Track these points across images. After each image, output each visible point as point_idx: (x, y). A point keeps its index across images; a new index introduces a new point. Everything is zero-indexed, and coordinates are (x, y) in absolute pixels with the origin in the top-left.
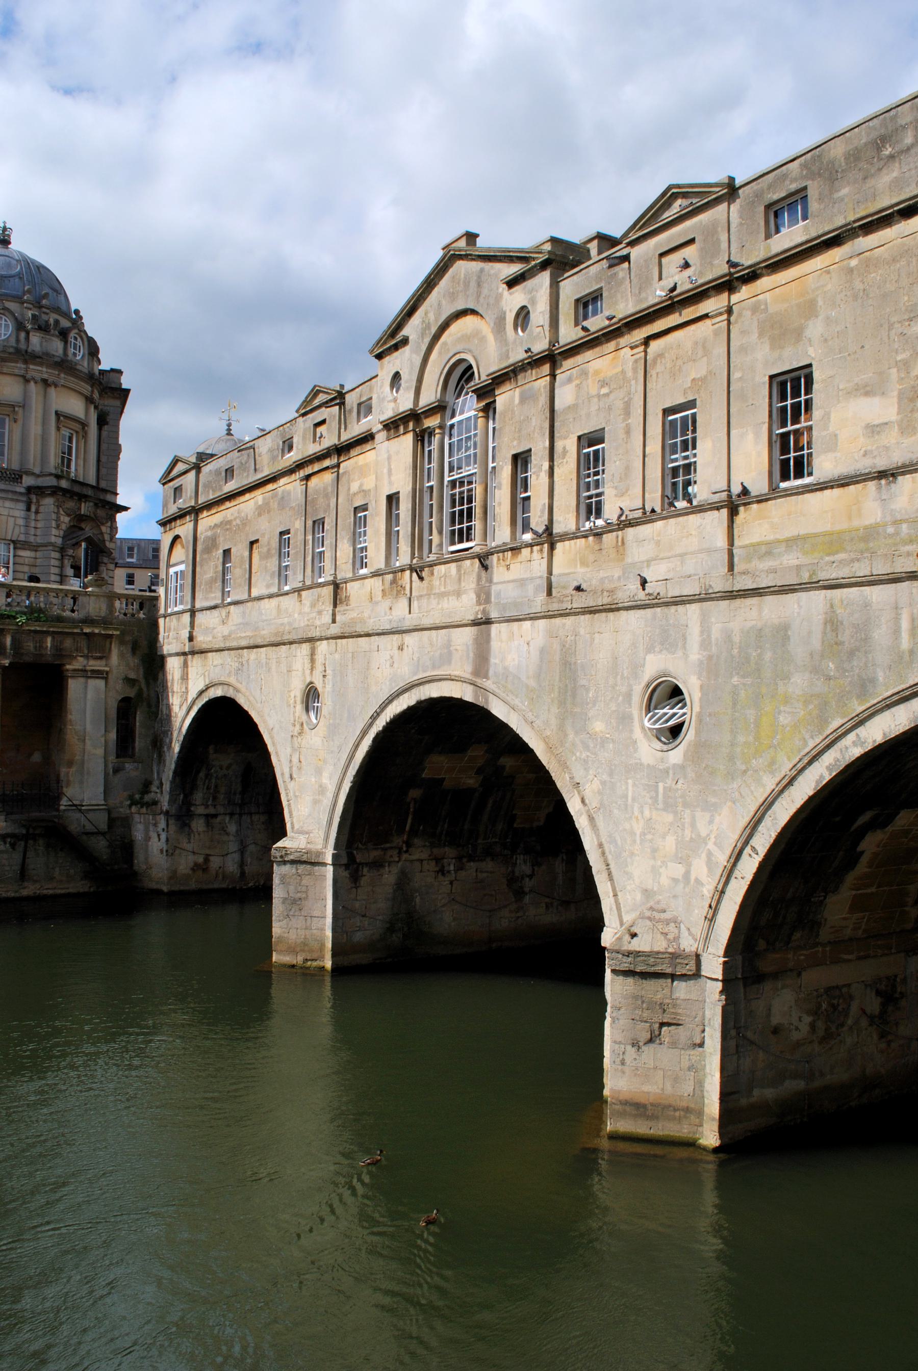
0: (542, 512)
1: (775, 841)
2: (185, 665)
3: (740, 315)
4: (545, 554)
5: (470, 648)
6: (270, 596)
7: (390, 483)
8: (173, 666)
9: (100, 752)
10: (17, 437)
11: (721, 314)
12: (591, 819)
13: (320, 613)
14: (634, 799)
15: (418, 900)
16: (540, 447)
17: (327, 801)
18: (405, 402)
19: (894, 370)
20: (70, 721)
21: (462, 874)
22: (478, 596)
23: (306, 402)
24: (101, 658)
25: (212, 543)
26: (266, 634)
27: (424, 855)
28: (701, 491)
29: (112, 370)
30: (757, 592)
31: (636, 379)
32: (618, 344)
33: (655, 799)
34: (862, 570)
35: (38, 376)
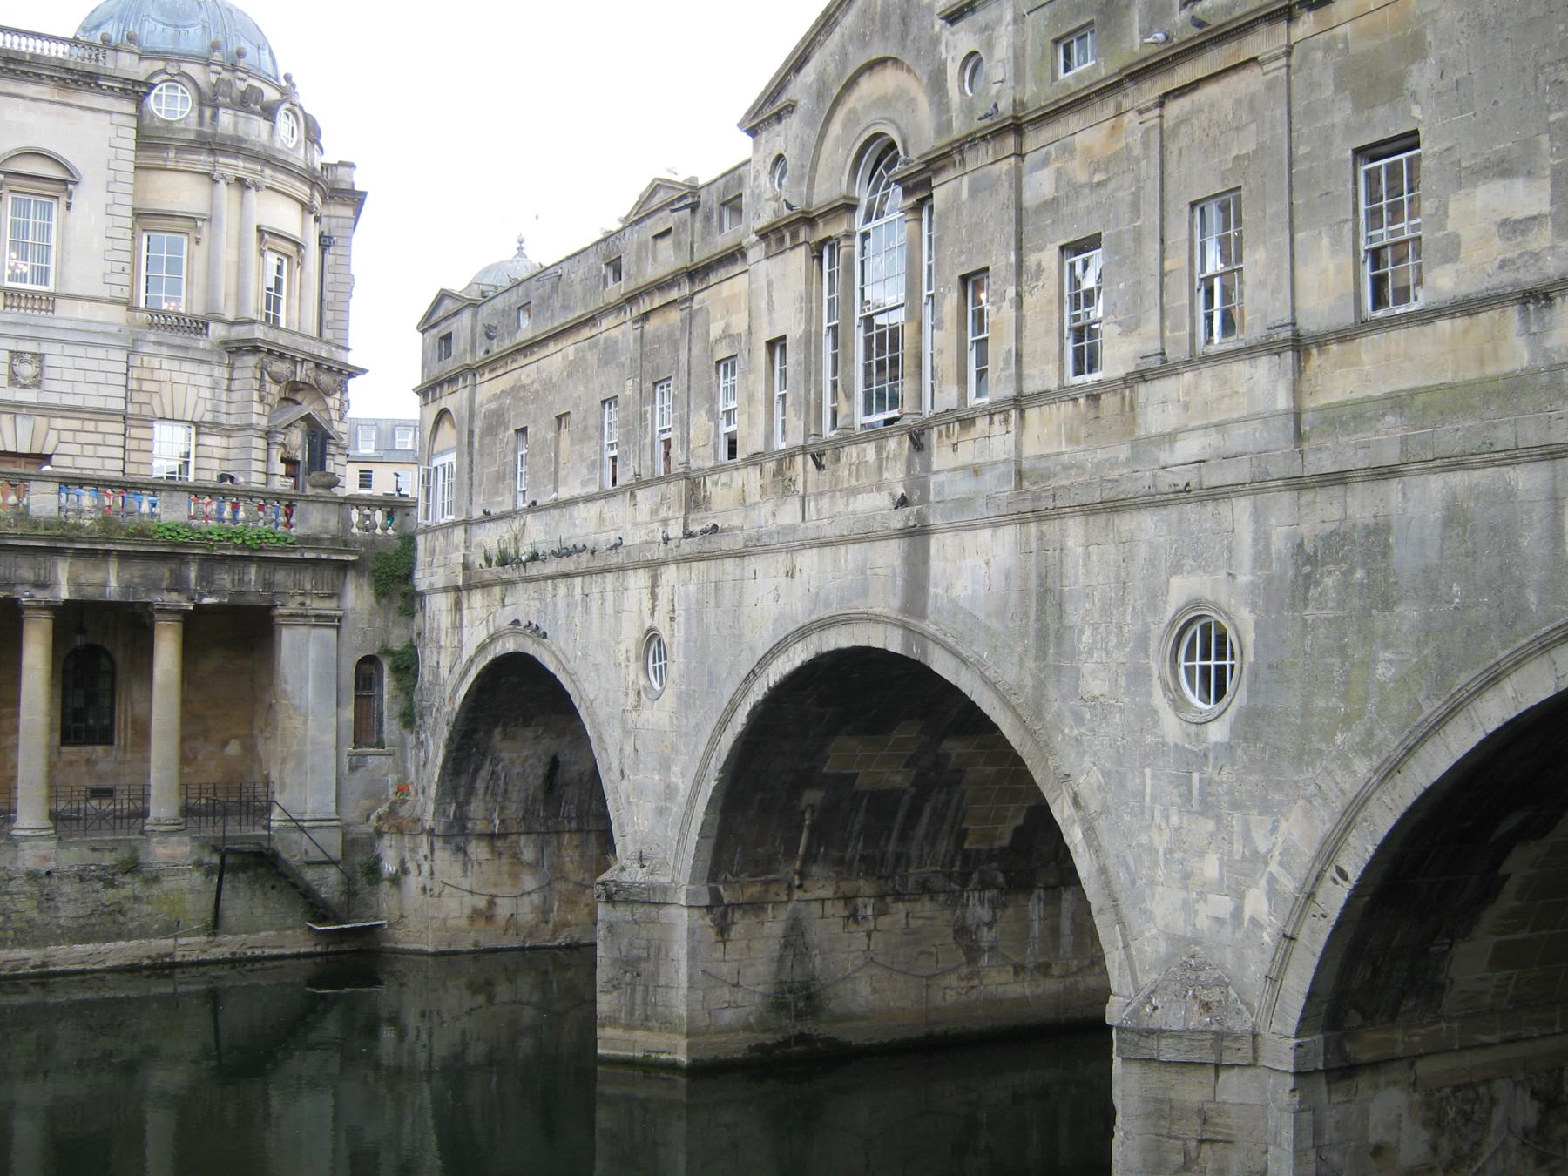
0: (1007, 361)
2: (458, 606)
3: (1305, 57)
4: (1012, 427)
5: (898, 571)
6: (589, 499)
7: (771, 323)
8: (439, 605)
9: (331, 738)
10: (200, 266)
11: (1277, 58)
12: (1090, 832)
14: (1154, 798)
15: (818, 961)
16: (1000, 260)
20: (285, 691)
21: (884, 921)
24: (330, 596)
25: (496, 421)
29: (342, 164)
31: (1147, 157)
32: (1119, 106)
33: (1188, 798)
35: (231, 173)
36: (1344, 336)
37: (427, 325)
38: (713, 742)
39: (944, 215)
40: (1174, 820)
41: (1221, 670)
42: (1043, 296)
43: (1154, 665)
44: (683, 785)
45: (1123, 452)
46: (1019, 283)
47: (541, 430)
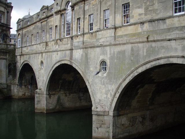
1: (122, 90)
2: (20, 57)
6: (35, 45)
8: (18, 57)
12: (90, 86)
13: (43, 48)
14: (98, 83)
16: (82, 17)
17: (44, 83)
18: (59, 8)
19: (144, 4)
21: (70, 96)
22: (71, 45)
23: (42, 9)
25: (25, 35)
26: (34, 52)
27: (63, 93)
28: (109, 25)
29: (10, 3)
30: (120, 44)
31: (99, 4)
33: (101, 83)
34: (138, 40)
36: (120, 27)
37: (17, 23)
38: (49, 75)
39: (75, 11)
40: (100, 85)
41: (106, 67)
42: (86, 21)
43: (98, 67)
44: (45, 80)
45: (95, 40)
46: (84, 19)
47: (30, 36)
